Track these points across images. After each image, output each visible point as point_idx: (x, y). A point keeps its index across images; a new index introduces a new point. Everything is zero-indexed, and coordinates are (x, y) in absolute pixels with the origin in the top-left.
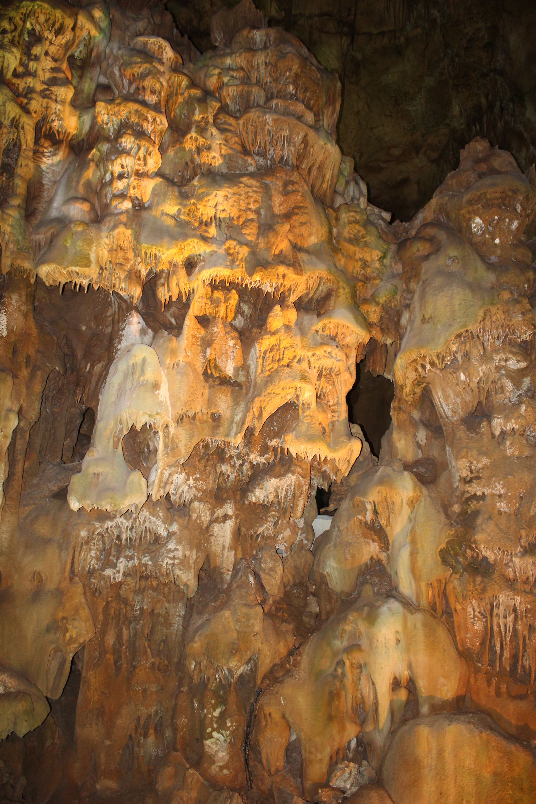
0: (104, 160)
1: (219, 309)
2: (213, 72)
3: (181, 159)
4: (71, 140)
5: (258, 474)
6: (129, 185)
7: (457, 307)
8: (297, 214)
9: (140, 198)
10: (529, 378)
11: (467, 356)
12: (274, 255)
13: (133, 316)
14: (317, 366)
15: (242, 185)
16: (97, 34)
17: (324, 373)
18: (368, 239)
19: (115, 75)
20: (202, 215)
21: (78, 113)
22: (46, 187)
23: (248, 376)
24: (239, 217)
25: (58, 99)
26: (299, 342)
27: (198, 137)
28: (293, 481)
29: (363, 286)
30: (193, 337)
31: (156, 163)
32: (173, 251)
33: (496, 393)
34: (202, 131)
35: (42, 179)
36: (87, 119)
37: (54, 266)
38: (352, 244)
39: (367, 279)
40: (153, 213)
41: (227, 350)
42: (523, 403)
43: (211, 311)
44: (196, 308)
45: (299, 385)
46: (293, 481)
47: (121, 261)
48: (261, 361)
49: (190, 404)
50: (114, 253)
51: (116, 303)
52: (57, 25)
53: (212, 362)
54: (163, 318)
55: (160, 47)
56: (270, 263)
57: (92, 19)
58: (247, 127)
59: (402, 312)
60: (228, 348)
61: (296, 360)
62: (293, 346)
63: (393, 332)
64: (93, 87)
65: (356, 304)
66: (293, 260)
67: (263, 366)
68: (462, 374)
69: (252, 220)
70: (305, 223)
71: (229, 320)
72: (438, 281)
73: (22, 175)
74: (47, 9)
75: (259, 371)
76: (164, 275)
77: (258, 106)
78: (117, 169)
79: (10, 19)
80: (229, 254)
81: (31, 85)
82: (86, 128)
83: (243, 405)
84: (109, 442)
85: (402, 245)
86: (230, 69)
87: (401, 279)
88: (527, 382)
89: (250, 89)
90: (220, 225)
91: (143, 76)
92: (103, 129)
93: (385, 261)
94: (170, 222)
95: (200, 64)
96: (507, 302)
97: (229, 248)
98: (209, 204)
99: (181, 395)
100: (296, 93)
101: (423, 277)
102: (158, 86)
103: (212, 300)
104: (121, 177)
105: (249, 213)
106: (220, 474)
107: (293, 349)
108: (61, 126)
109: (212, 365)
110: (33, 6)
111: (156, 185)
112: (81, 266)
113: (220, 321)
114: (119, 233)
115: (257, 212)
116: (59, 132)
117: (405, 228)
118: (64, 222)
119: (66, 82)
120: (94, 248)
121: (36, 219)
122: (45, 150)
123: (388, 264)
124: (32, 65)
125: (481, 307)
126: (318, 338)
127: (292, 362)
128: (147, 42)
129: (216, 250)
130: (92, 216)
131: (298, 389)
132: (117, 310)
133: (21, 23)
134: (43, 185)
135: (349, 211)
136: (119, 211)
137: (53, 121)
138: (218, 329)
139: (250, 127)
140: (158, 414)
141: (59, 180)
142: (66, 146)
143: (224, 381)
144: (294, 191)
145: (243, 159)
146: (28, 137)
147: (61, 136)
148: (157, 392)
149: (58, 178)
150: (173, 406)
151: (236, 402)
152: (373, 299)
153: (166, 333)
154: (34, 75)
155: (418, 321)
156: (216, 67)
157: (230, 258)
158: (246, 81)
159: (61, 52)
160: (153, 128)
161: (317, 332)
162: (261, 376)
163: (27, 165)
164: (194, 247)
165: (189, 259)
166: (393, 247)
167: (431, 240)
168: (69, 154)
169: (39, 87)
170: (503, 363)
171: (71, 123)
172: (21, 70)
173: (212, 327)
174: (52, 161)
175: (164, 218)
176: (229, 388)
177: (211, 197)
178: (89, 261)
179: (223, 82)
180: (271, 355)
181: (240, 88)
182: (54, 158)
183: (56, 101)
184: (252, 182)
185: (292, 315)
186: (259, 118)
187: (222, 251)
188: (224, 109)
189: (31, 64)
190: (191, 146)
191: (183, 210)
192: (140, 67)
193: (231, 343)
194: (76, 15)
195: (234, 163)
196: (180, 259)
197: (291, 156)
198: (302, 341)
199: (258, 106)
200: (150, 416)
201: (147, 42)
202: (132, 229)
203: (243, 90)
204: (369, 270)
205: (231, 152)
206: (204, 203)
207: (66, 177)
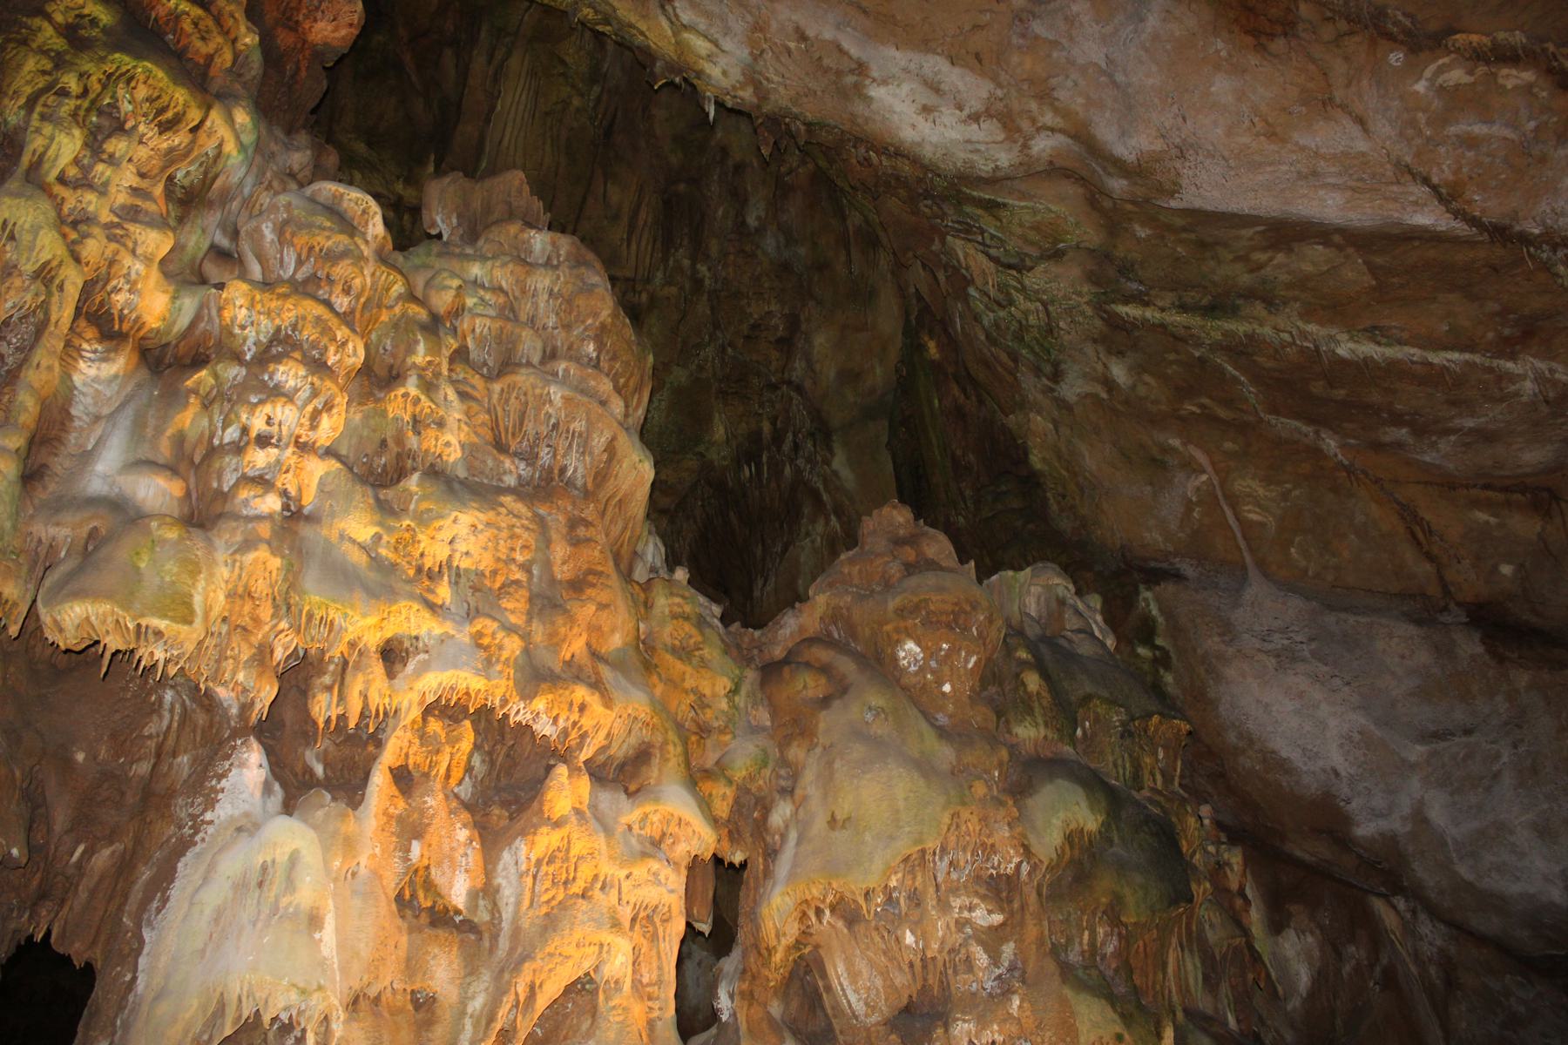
0: (224, 400)
1: (440, 757)
2: (448, 282)
3: (374, 431)
4: (143, 338)
7: (901, 804)
8: (593, 585)
9: (293, 493)
10: (1012, 945)
11: (916, 899)
12: (564, 662)
14: (633, 901)
15: (503, 510)
16: (235, 153)
17: (642, 914)
18: (706, 652)
19: (263, 236)
20: (422, 555)
21: (171, 289)
22: (77, 423)
23: (495, 909)
24: (495, 573)
25: (139, 251)
26: (604, 847)
27: (423, 397)
29: (698, 742)
31: (334, 430)
32: (372, 620)
33: (956, 972)
35: (70, 404)
36: (189, 304)
37: (106, 607)
38: (680, 659)
39: (703, 731)
40: (325, 532)
41: (452, 849)
42: (1014, 993)
43: (419, 760)
47: (246, 621)
48: (529, 880)
49: (377, 968)
50: (239, 602)
51: (178, 709)
52: (169, 114)
53: (421, 873)
54: (321, 764)
55: (364, 212)
56: (559, 678)
57: (230, 120)
58: (507, 401)
59: (773, 801)
60: (455, 845)
61: (599, 885)
63: (749, 840)
64: (205, 246)
65: (695, 778)
66: (589, 673)
68: (908, 933)
69: (517, 582)
71: (453, 782)
72: (858, 751)
73: (36, 385)
74: (160, 80)
75: (526, 903)
76: (332, 667)
77: (529, 364)
78: (258, 425)
79: (82, 76)
80: (479, 646)
81: (91, 208)
82: (183, 322)
83: (486, 976)
85: (771, 672)
86: (476, 284)
87: (772, 737)
88: (1008, 950)
90: (457, 583)
91: (332, 257)
92: (231, 334)
93: (737, 699)
94: (358, 558)
95: (417, 261)
96: (983, 801)
97: (480, 635)
98: (440, 536)
99: (362, 945)
100: (598, 357)
101: (822, 739)
103: (423, 736)
104: (263, 441)
105: (513, 567)
107: (594, 862)
108: (128, 303)
109: (419, 880)
110: (135, 67)
111: (327, 474)
112: (173, 619)
113: (438, 786)
114: (256, 560)
115: (526, 568)
116: (122, 319)
117: (753, 640)
118: (125, 515)
120: (201, 585)
121: (45, 488)
122: (85, 346)
123: (742, 705)
125: (945, 808)
126: (634, 841)
128: (342, 195)
129: (452, 632)
130: (186, 510)
132: (175, 725)
133: (97, 87)
134: (70, 417)
135: (672, 594)
136: (252, 513)
137: (117, 290)
138: (434, 801)
139: (513, 400)
140: (320, 988)
141: (112, 415)
142: (133, 349)
143: (442, 918)
144: (588, 540)
145: (495, 459)
146: (63, 313)
147: (125, 327)
148: (317, 936)
149: (106, 411)
150: (344, 970)
151: (471, 969)
152: (717, 772)
153: (328, 797)
155: (819, 824)
156: (454, 275)
157: (482, 654)
158: (508, 312)
160: (338, 357)
161: (630, 828)
162: (531, 913)
163: (50, 368)
164: (408, 619)
165: (388, 641)
166: (751, 675)
167: (825, 670)
168: (137, 367)
169: (106, 216)
170: (966, 914)
171: (154, 305)
172: (73, 172)
173: (422, 796)
174: (99, 373)
175: (347, 546)
176: (457, 937)
177: (448, 522)
178: (192, 612)
179: (463, 306)
180: (551, 869)
181: (498, 324)
182: (104, 365)
183: (133, 252)
184: (520, 507)
186: (534, 387)
187: (464, 636)
188: (460, 355)
189: (100, 167)
190: (400, 413)
191: (385, 538)
192: (328, 238)
193: (463, 834)
194: (209, 108)
195: (477, 463)
196: (373, 640)
197: (580, 471)
198: (608, 844)
199: (529, 364)
200: (303, 992)
201: (342, 195)
202: (283, 557)
203: (502, 329)
204: (709, 713)
205: (475, 439)
207: (129, 411)
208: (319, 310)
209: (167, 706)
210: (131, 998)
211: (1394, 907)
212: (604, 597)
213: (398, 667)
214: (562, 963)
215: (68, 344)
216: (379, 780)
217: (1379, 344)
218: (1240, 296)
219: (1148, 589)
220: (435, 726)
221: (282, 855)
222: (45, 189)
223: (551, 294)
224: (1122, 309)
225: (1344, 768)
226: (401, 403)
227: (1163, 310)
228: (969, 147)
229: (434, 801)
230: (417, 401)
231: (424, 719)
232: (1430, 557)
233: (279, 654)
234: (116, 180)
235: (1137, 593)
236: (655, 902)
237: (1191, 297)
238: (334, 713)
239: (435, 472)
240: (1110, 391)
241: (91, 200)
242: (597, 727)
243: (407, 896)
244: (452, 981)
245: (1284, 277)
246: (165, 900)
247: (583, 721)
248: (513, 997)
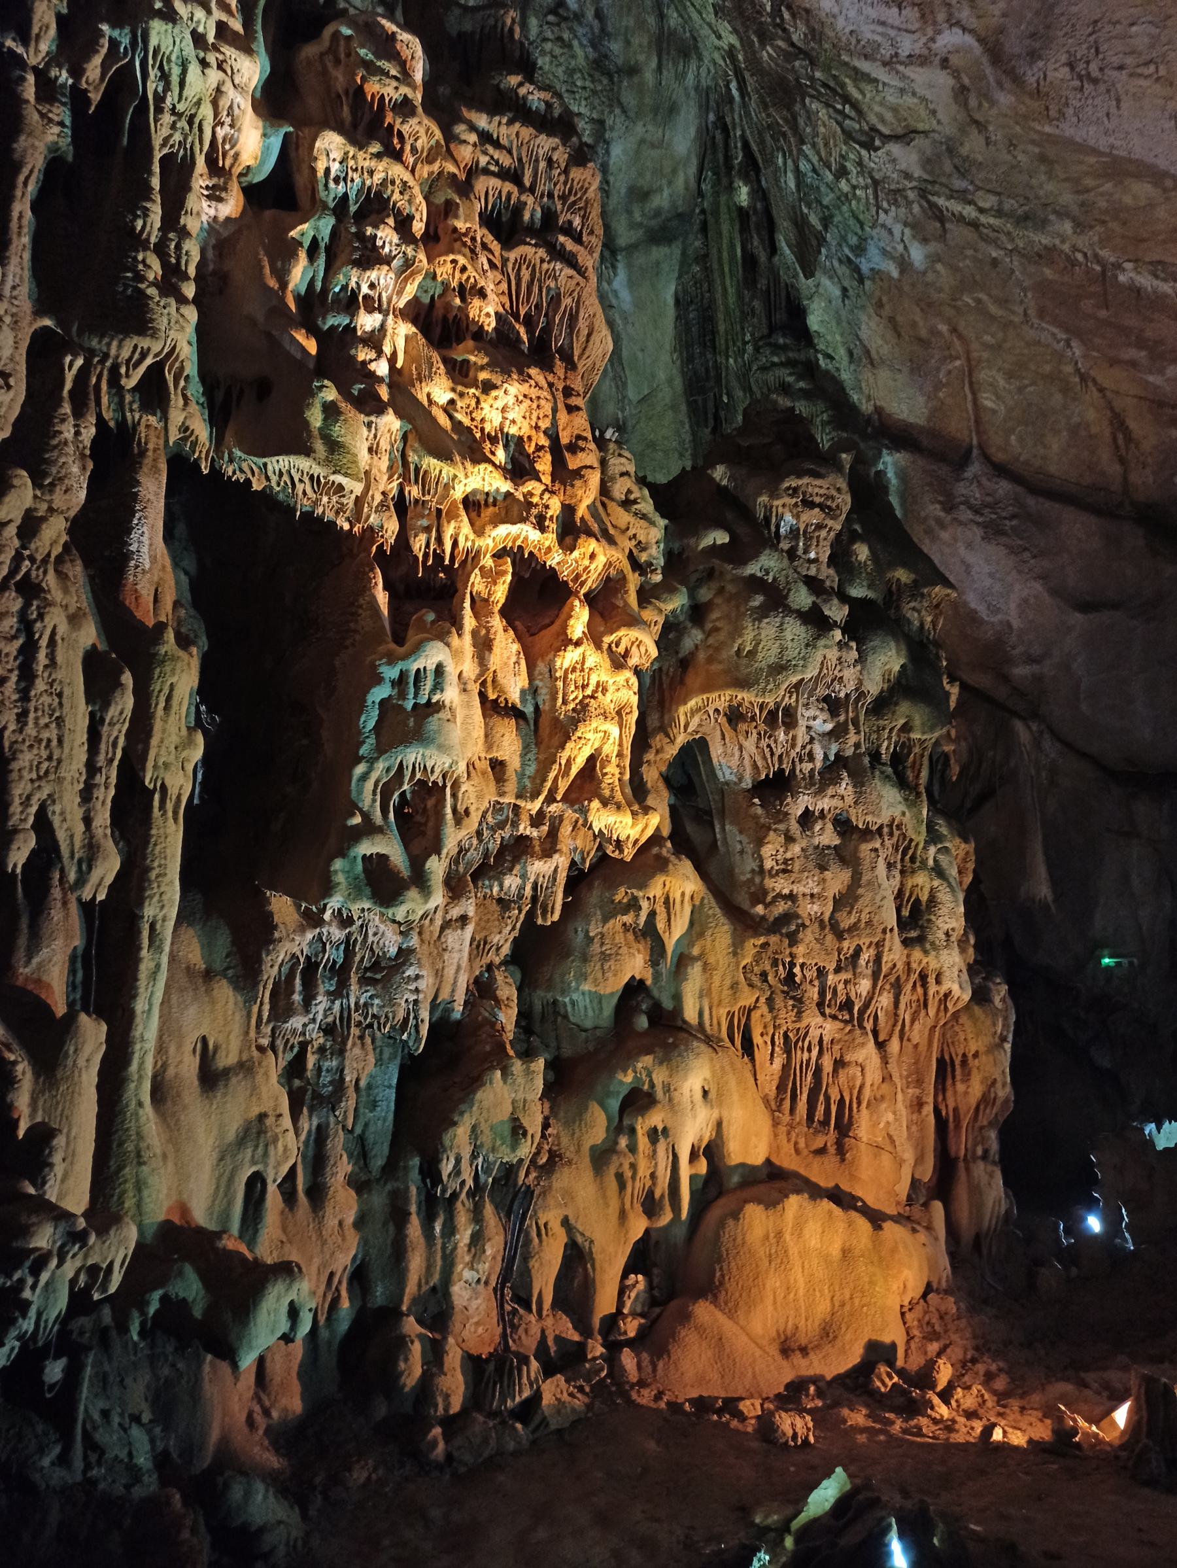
8: (583, 450)
84: (374, 801)
97: (531, 494)
211: (1029, 727)
217: (1156, 277)
218: (1055, 212)
219: (890, 454)
221: (431, 665)
224: (941, 201)
225: (1016, 623)
227: (981, 211)
228: (880, 29)
230: (464, 269)
232: (1122, 461)
235: (880, 455)
237: (1009, 204)
240: (902, 272)
245: (1103, 204)
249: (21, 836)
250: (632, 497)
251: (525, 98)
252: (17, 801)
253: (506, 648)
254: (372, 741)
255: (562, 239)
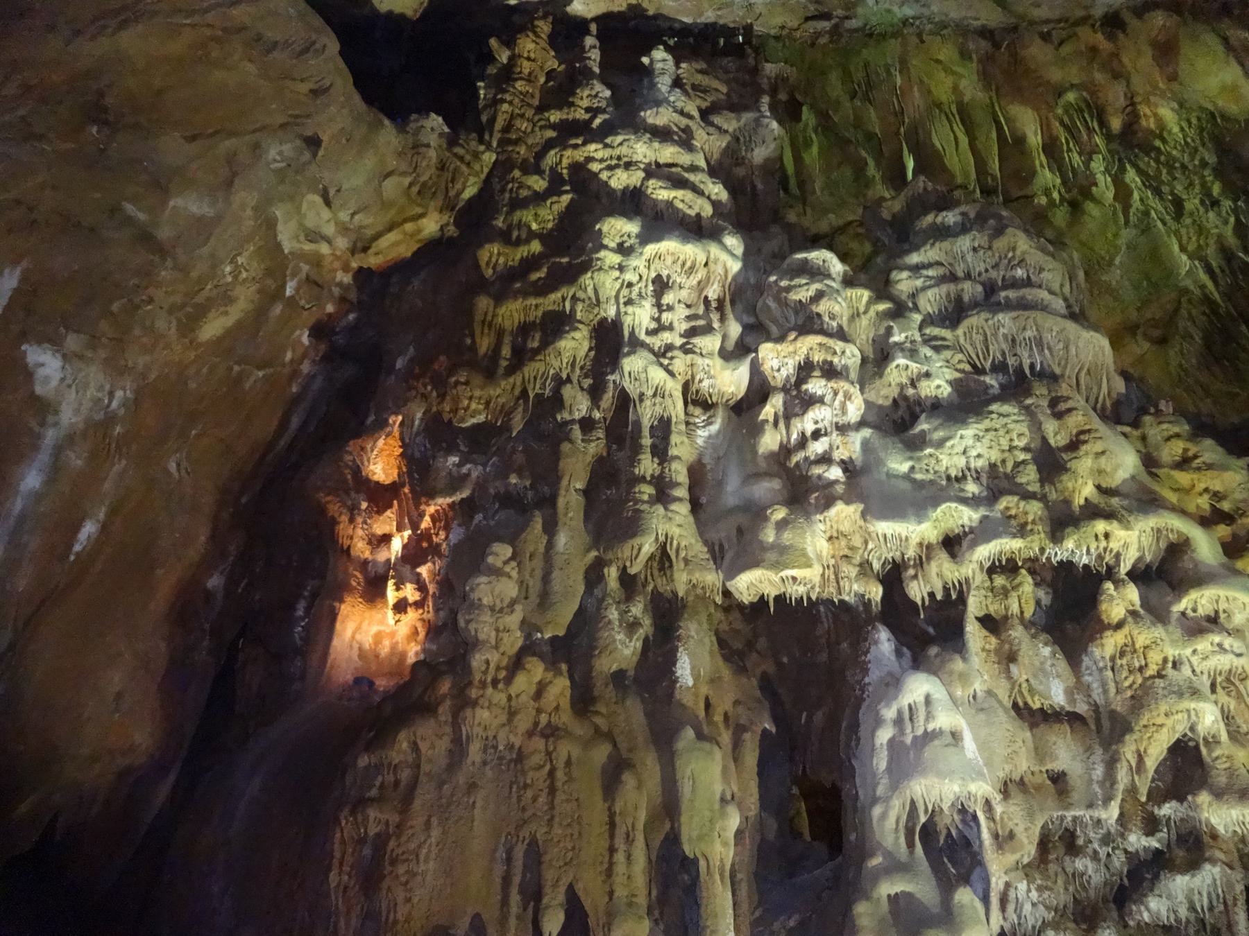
5: (1144, 872)
6: (831, 446)
8: (1086, 442)
13: (878, 631)
15: (994, 416)
17: (1219, 679)
22: (709, 467)
24: (1004, 461)
26: (1164, 635)
28: (1218, 877)
30: (983, 650)
34: (913, 354)
41: (1042, 663)
43: (996, 606)
44: (975, 605)
45: (1193, 705)
46: (1218, 877)
47: (846, 552)
51: (830, 615)
54: (931, 631)
61: (1170, 665)
62: (1159, 644)
67: (1116, 682)
69: (1023, 462)
70: (1103, 453)
75: (1113, 690)
84: (897, 838)
89: (960, 287)
97: (1007, 508)
102: (837, 308)
104: (817, 435)
105: (1017, 453)
106: (1074, 875)
107: (1159, 648)
108: (712, 386)
113: (1017, 621)
114: (838, 514)
119: (708, 330)
120: (809, 539)
124: (666, 317)
127: (1164, 669)
131: (1193, 713)
135: (1160, 423)
138: (1017, 633)
141: (725, 454)
147: (714, 399)
154: (670, 328)
159: (694, 295)
175: (893, 481)
178: (809, 559)
180: (1124, 662)
184: (1006, 408)
185: (1132, 594)
186: (987, 320)
193: (1046, 651)
206: (946, 450)
208: (819, 339)
209: (823, 615)
210: (859, 805)
212: (1098, 447)
213: (957, 548)
214: (1157, 731)
215: (687, 423)
216: (973, 630)
220: (999, 581)
222: (643, 345)
223: (975, 249)
226: (899, 370)
229: (1017, 633)
231: (991, 580)
233: (876, 566)
234: (676, 318)
236: (1227, 667)
238: (926, 590)
239: (935, 407)
241: (667, 337)
242: (1126, 546)
243: (1021, 704)
244: (1073, 758)
246: (858, 740)
247: (1111, 545)
248: (1125, 764)
249: (550, 910)
250: (1190, 454)
251: (942, 223)
252: (549, 883)
253: (1039, 654)
254: (885, 781)
255: (1003, 294)
